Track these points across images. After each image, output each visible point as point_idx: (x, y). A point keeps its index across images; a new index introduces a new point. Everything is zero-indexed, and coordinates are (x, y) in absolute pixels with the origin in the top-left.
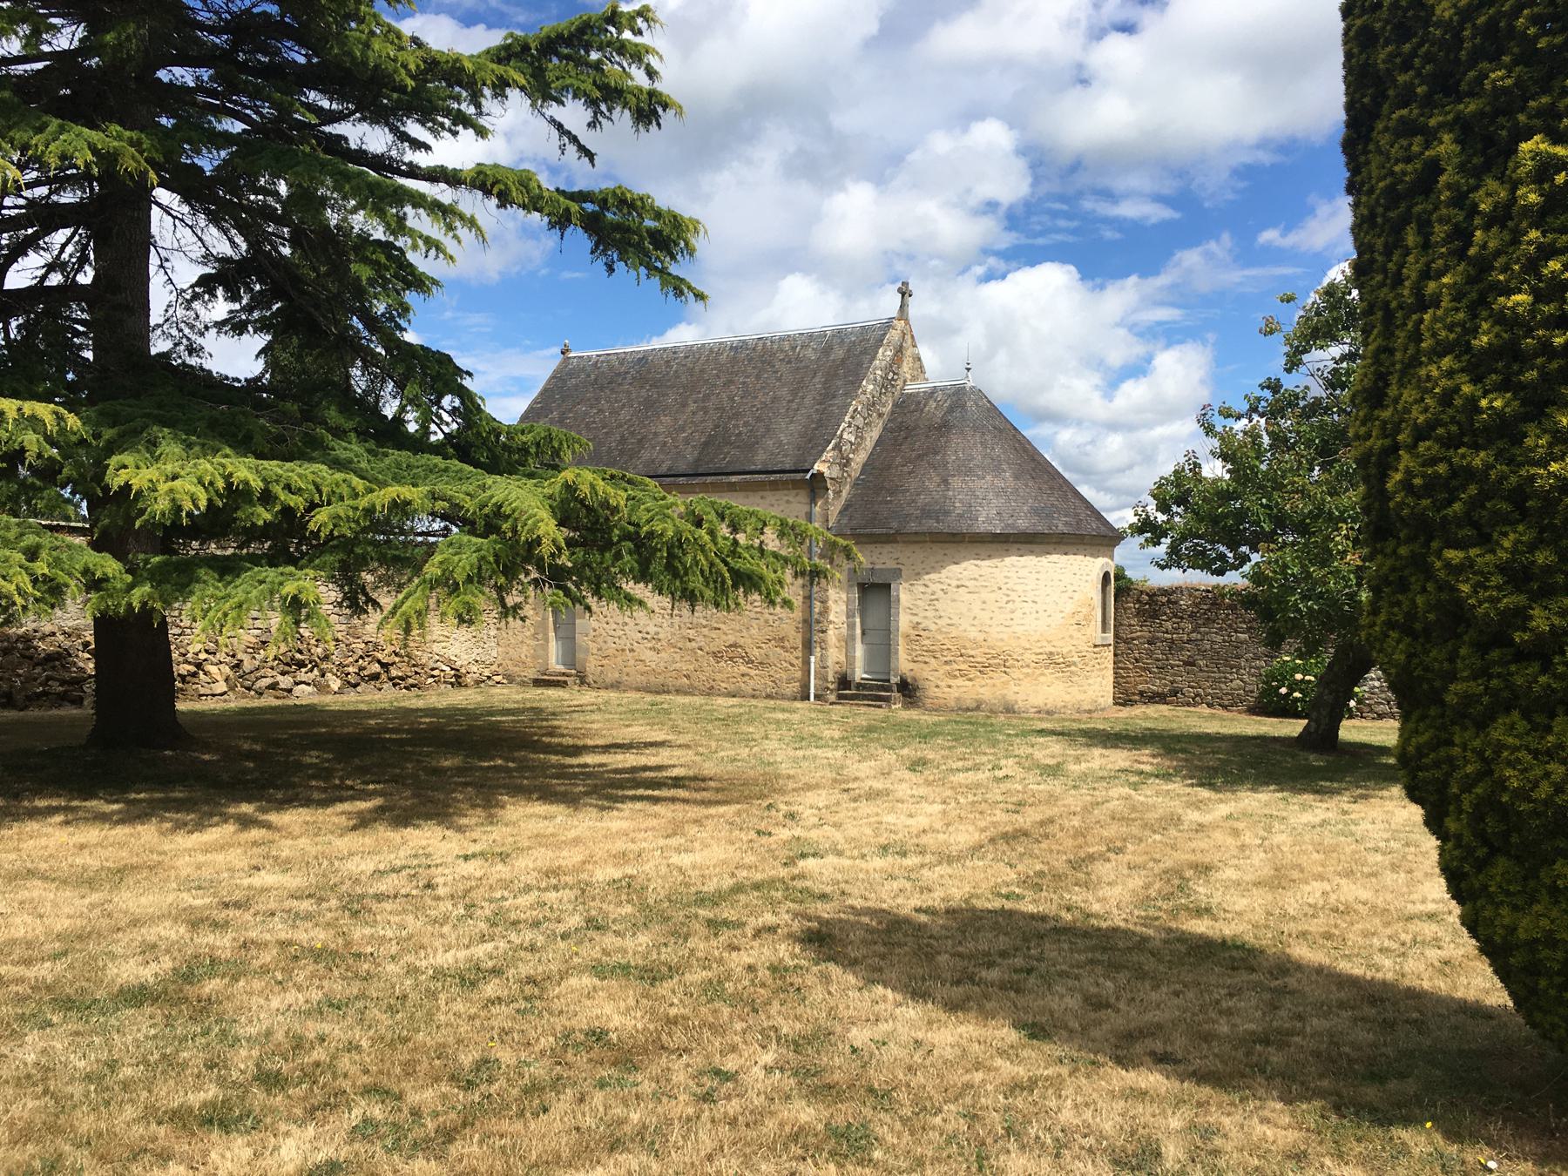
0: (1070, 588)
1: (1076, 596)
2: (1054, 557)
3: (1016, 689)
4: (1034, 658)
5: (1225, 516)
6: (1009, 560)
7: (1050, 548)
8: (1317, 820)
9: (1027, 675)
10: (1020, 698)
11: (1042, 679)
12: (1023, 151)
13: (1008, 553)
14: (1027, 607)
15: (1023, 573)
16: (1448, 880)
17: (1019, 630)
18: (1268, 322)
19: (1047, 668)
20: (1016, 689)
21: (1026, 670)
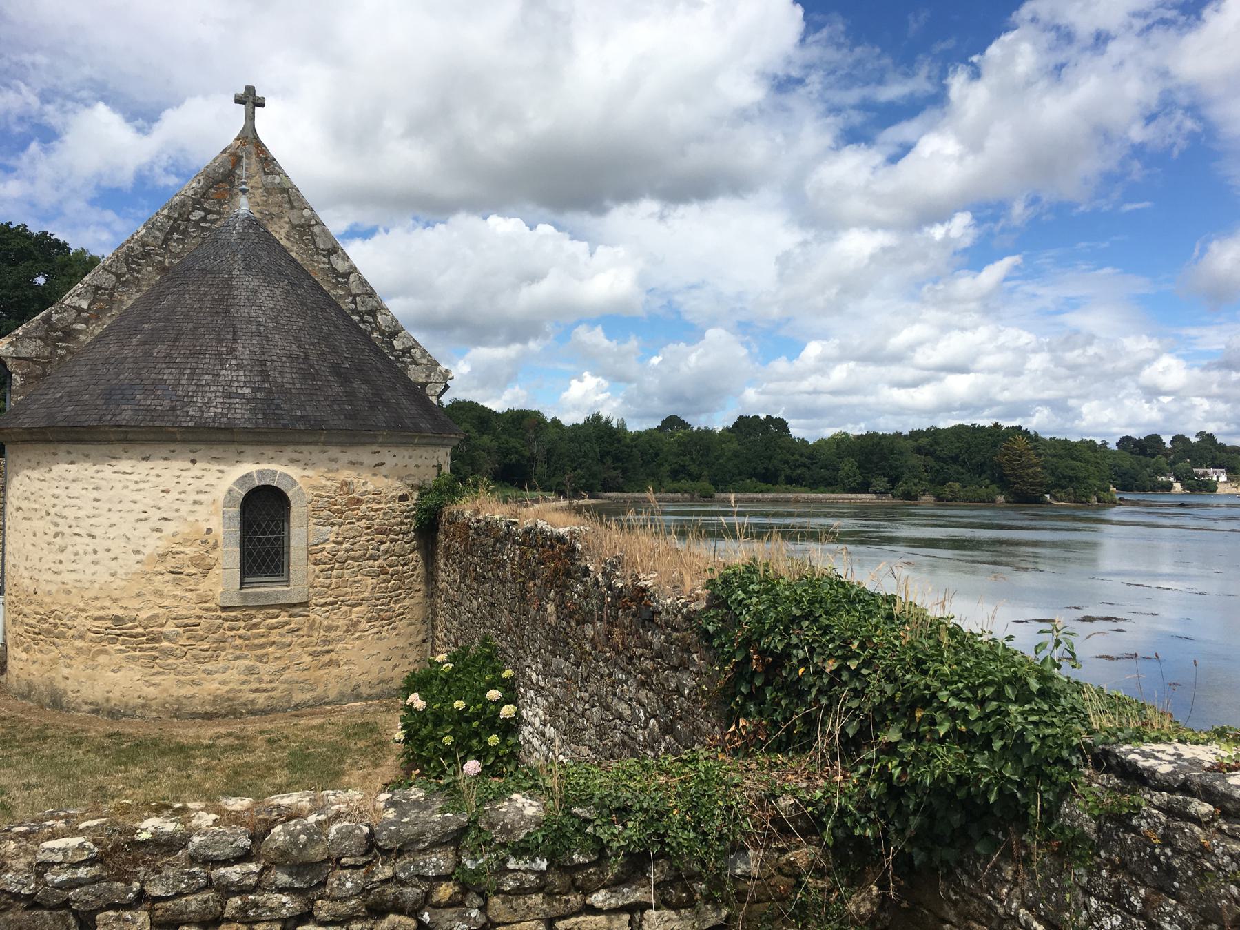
0: (155, 515)
1: (169, 528)
2: (124, 465)
3: (66, 671)
4: (89, 624)
5: (968, 700)
6: (60, 469)
7: (117, 449)
8: (636, 221)
9: (80, 651)
10: (71, 685)
11: (102, 659)
12: (885, 166)
13: (55, 458)
14: (82, 543)
15: (76, 489)
16: (1075, 445)
17: (69, 578)
18: (250, 90)
19: (113, 641)
20: (66, 671)
21: (78, 643)
